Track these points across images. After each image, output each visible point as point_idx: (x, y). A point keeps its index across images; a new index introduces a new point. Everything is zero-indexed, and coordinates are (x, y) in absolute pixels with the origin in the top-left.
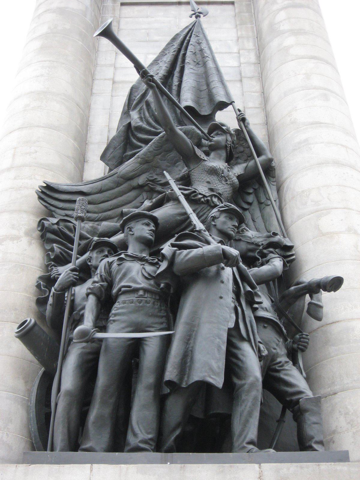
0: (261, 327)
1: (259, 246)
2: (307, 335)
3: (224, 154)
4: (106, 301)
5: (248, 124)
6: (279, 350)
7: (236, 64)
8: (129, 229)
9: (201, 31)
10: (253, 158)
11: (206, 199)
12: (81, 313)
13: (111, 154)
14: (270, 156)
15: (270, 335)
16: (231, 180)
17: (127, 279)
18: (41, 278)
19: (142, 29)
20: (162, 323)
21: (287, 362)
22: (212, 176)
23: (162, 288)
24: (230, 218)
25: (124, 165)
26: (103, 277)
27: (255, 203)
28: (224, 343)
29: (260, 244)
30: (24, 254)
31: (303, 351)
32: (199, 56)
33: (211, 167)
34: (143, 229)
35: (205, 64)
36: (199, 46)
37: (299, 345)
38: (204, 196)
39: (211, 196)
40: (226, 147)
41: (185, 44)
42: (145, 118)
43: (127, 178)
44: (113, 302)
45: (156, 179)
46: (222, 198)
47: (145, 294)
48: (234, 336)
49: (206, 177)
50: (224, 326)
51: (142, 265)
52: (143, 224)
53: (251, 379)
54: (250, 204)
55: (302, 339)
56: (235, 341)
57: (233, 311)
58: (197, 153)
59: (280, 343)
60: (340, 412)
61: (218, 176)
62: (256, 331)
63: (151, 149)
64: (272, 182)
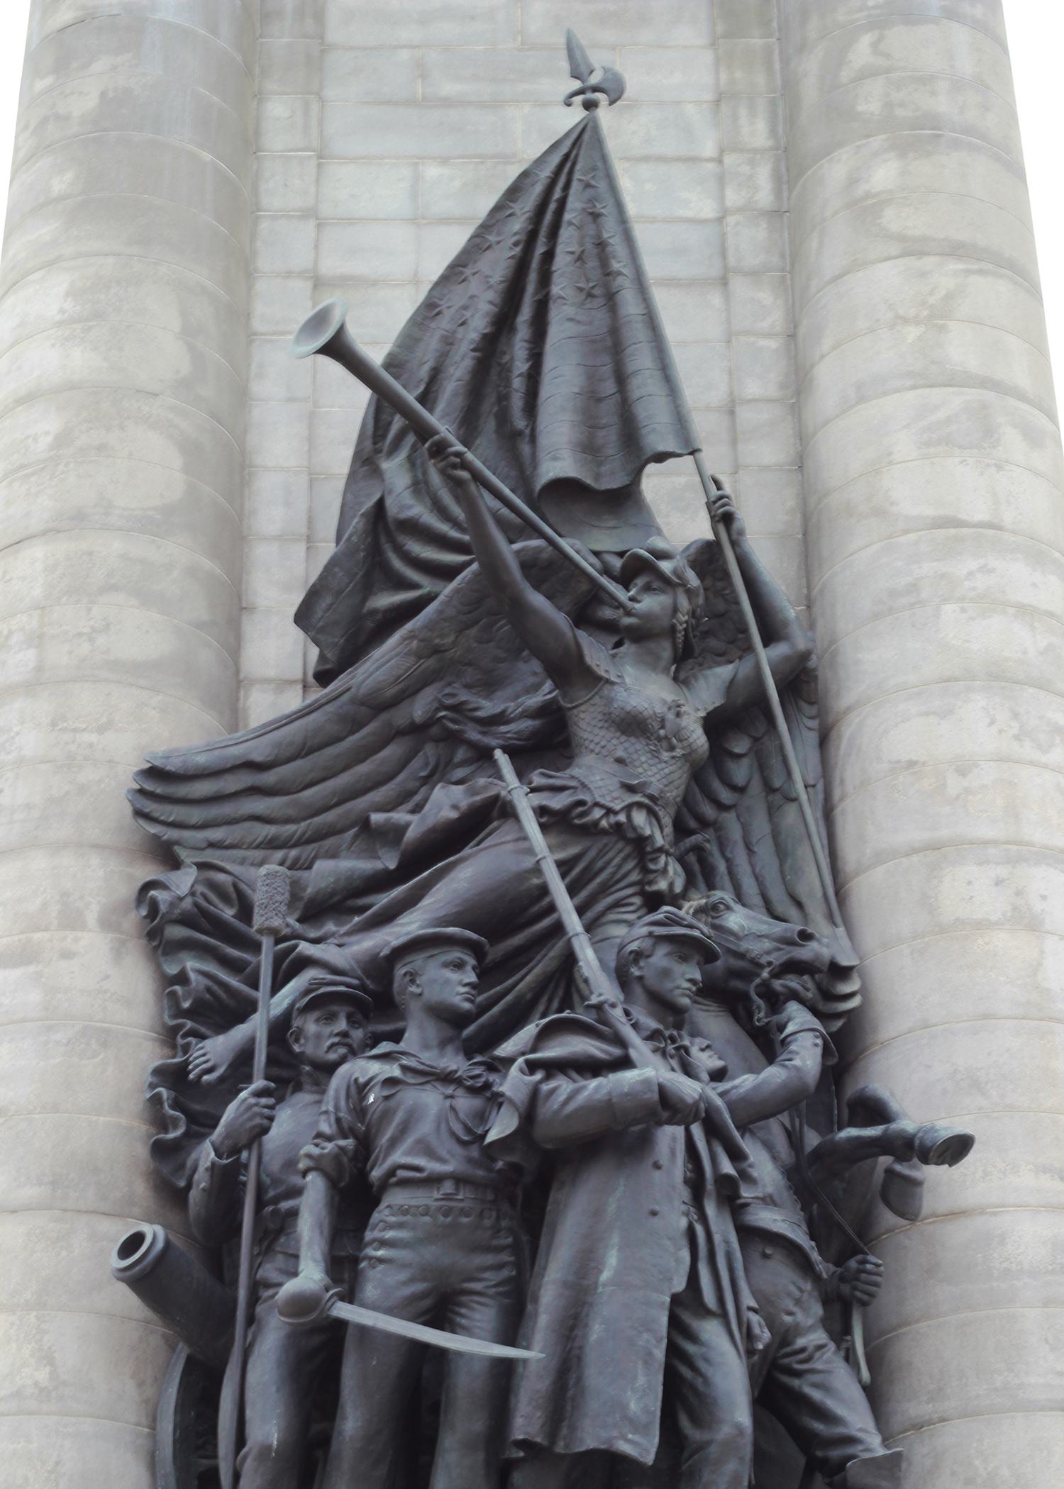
0: (755, 1255)
1: (761, 967)
2: (878, 1265)
3: (665, 650)
4: (355, 1198)
5: (741, 533)
6: (800, 1317)
7: (708, 209)
8: (408, 978)
9: (599, 164)
10: (749, 648)
11: (613, 819)
12: (285, 1205)
13: (328, 609)
14: (801, 644)
15: (780, 1276)
16: (685, 743)
17: (409, 1141)
18: (158, 1072)
19: (396, 47)
20: (499, 1267)
21: (820, 1347)
22: (633, 740)
23: (499, 1171)
24: (680, 957)
25: (372, 660)
26: (345, 1126)
27: (756, 787)
28: (659, 1341)
29: (764, 960)
30: (105, 992)
31: (864, 1304)
32: (592, 263)
33: (628, 713)
34: (447, 982)
35: (611, 300)
36: (593, 227)
37: (855, 1288)
38: (609, 811)
39: (628, 808)
40: (673, 630)
41: (548, 217)
42: (427, 483)
43: (377, 705)
44: (376, 1202)
45: (464, 703)
46: (657, 809)
47: (457, 1189)
48: (685, 1306)
49: (615, 741)
50: (662, 1293)
51: (447, 1097)
52: (446, 965)
53: (725, 1431)
54: (741, 790)
55: (863, 1275)
56: (687, 1317)
57: (684, 1243)
58: (588, 659)
59: (805, 1297)
60: (953, 1473)
61: (648, 738)
62: (740, 1273)
63: (450, 612)
64: (805, 720)
